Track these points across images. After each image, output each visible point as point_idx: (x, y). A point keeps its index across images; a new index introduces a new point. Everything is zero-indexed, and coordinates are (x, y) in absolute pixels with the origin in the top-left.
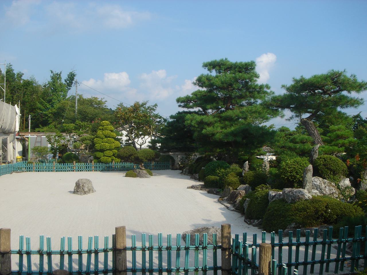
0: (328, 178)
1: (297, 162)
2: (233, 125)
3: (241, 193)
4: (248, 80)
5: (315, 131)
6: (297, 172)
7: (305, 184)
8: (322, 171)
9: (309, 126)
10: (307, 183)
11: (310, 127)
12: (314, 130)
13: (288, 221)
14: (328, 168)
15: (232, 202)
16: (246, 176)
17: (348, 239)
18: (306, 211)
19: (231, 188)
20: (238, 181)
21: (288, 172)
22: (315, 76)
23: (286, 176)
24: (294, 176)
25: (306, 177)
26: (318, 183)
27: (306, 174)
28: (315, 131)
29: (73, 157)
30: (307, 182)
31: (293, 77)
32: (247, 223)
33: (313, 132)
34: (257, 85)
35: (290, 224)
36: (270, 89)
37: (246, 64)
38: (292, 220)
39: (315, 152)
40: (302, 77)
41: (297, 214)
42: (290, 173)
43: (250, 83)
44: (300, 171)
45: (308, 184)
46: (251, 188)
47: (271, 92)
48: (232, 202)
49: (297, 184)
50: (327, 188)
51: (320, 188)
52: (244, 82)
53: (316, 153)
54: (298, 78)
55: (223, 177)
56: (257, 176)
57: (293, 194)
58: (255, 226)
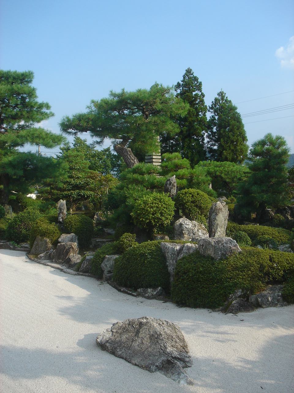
0: (196, 219)
1: (158, 199)
2: (9, 153)
3: (73, 246)
4: (25, 96)
5: (135, 160)
6: (161, 213)
7: (214, 229)
8: (190, 210)
9: (127, 153)
10: (217, 228)
11: (129, 155)
12: (133, 159)
13: (230, 288)
14: (196, 206)
15: (61, 261)
16: (70, 222)
17: (133, 293)
18: (250, 270)
19: (48, 240)
20: (57, 229)
21: (149, 213)
22: (139, 91)
23: (147, 219)
24: (158, 218)
25: (216, 219)
26: (190, 226)
27: (217, 214)
28: (135, 160)
29: (223, 127)
30: (217, 226)
31: (111, 90)
32: (133, 295)
33: (133, 162)
34: (37, 103)
35: (234, 292)
36: (50, 109)
37: (23, 75)
38: (235, 285)
39: (173, 185)
40: (123, 90)
41: (238, 275)
42: (153, 214)
43: (27, 100)
44: (165, 211)
45: (219, 229)
46: (77, 238)
47: (51, 113)
48: (61, 261)
49: (157, 229)
50: (200, 232)
51: (193, 233)
52: (20, 97)
53: (174, 187)
54: (118, 91)
55: (16, 224)
56: (85, 220)
57: (224, 246)
58: (152, 299)
